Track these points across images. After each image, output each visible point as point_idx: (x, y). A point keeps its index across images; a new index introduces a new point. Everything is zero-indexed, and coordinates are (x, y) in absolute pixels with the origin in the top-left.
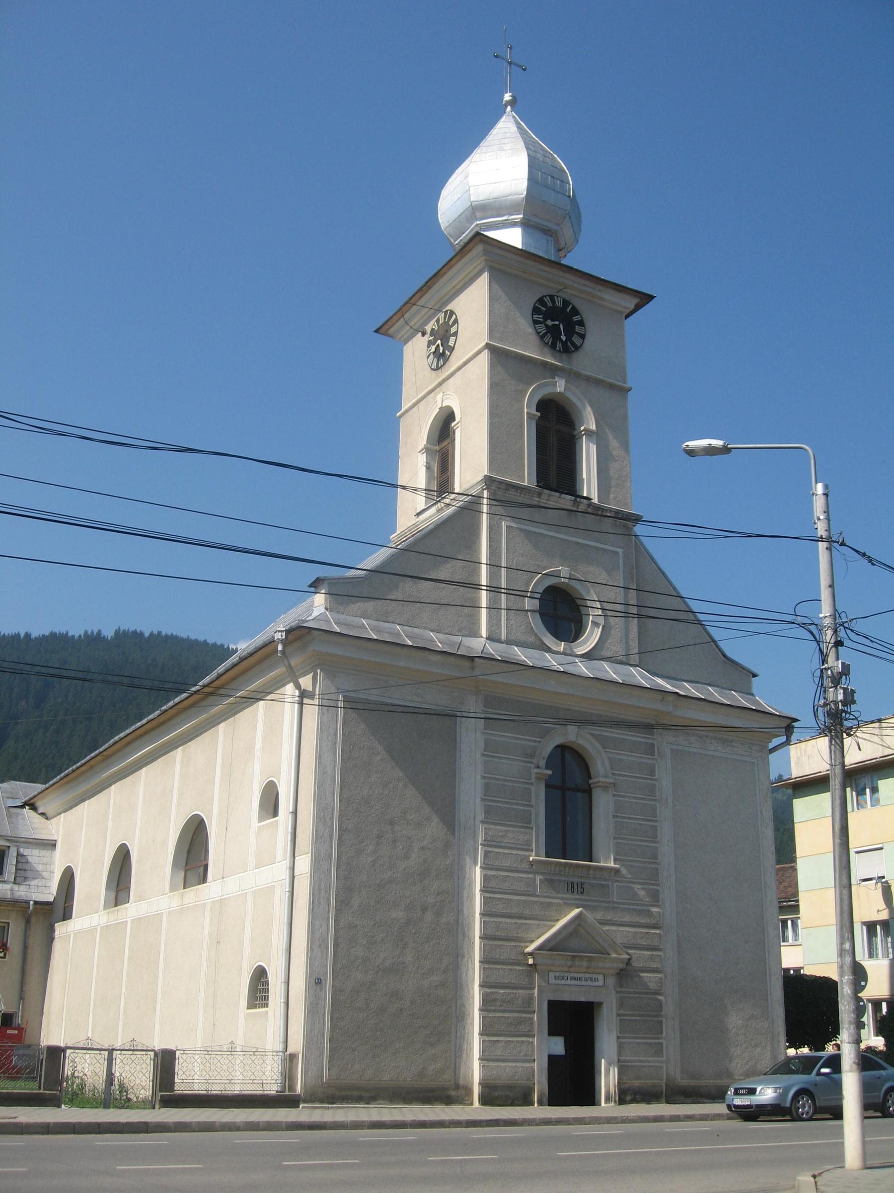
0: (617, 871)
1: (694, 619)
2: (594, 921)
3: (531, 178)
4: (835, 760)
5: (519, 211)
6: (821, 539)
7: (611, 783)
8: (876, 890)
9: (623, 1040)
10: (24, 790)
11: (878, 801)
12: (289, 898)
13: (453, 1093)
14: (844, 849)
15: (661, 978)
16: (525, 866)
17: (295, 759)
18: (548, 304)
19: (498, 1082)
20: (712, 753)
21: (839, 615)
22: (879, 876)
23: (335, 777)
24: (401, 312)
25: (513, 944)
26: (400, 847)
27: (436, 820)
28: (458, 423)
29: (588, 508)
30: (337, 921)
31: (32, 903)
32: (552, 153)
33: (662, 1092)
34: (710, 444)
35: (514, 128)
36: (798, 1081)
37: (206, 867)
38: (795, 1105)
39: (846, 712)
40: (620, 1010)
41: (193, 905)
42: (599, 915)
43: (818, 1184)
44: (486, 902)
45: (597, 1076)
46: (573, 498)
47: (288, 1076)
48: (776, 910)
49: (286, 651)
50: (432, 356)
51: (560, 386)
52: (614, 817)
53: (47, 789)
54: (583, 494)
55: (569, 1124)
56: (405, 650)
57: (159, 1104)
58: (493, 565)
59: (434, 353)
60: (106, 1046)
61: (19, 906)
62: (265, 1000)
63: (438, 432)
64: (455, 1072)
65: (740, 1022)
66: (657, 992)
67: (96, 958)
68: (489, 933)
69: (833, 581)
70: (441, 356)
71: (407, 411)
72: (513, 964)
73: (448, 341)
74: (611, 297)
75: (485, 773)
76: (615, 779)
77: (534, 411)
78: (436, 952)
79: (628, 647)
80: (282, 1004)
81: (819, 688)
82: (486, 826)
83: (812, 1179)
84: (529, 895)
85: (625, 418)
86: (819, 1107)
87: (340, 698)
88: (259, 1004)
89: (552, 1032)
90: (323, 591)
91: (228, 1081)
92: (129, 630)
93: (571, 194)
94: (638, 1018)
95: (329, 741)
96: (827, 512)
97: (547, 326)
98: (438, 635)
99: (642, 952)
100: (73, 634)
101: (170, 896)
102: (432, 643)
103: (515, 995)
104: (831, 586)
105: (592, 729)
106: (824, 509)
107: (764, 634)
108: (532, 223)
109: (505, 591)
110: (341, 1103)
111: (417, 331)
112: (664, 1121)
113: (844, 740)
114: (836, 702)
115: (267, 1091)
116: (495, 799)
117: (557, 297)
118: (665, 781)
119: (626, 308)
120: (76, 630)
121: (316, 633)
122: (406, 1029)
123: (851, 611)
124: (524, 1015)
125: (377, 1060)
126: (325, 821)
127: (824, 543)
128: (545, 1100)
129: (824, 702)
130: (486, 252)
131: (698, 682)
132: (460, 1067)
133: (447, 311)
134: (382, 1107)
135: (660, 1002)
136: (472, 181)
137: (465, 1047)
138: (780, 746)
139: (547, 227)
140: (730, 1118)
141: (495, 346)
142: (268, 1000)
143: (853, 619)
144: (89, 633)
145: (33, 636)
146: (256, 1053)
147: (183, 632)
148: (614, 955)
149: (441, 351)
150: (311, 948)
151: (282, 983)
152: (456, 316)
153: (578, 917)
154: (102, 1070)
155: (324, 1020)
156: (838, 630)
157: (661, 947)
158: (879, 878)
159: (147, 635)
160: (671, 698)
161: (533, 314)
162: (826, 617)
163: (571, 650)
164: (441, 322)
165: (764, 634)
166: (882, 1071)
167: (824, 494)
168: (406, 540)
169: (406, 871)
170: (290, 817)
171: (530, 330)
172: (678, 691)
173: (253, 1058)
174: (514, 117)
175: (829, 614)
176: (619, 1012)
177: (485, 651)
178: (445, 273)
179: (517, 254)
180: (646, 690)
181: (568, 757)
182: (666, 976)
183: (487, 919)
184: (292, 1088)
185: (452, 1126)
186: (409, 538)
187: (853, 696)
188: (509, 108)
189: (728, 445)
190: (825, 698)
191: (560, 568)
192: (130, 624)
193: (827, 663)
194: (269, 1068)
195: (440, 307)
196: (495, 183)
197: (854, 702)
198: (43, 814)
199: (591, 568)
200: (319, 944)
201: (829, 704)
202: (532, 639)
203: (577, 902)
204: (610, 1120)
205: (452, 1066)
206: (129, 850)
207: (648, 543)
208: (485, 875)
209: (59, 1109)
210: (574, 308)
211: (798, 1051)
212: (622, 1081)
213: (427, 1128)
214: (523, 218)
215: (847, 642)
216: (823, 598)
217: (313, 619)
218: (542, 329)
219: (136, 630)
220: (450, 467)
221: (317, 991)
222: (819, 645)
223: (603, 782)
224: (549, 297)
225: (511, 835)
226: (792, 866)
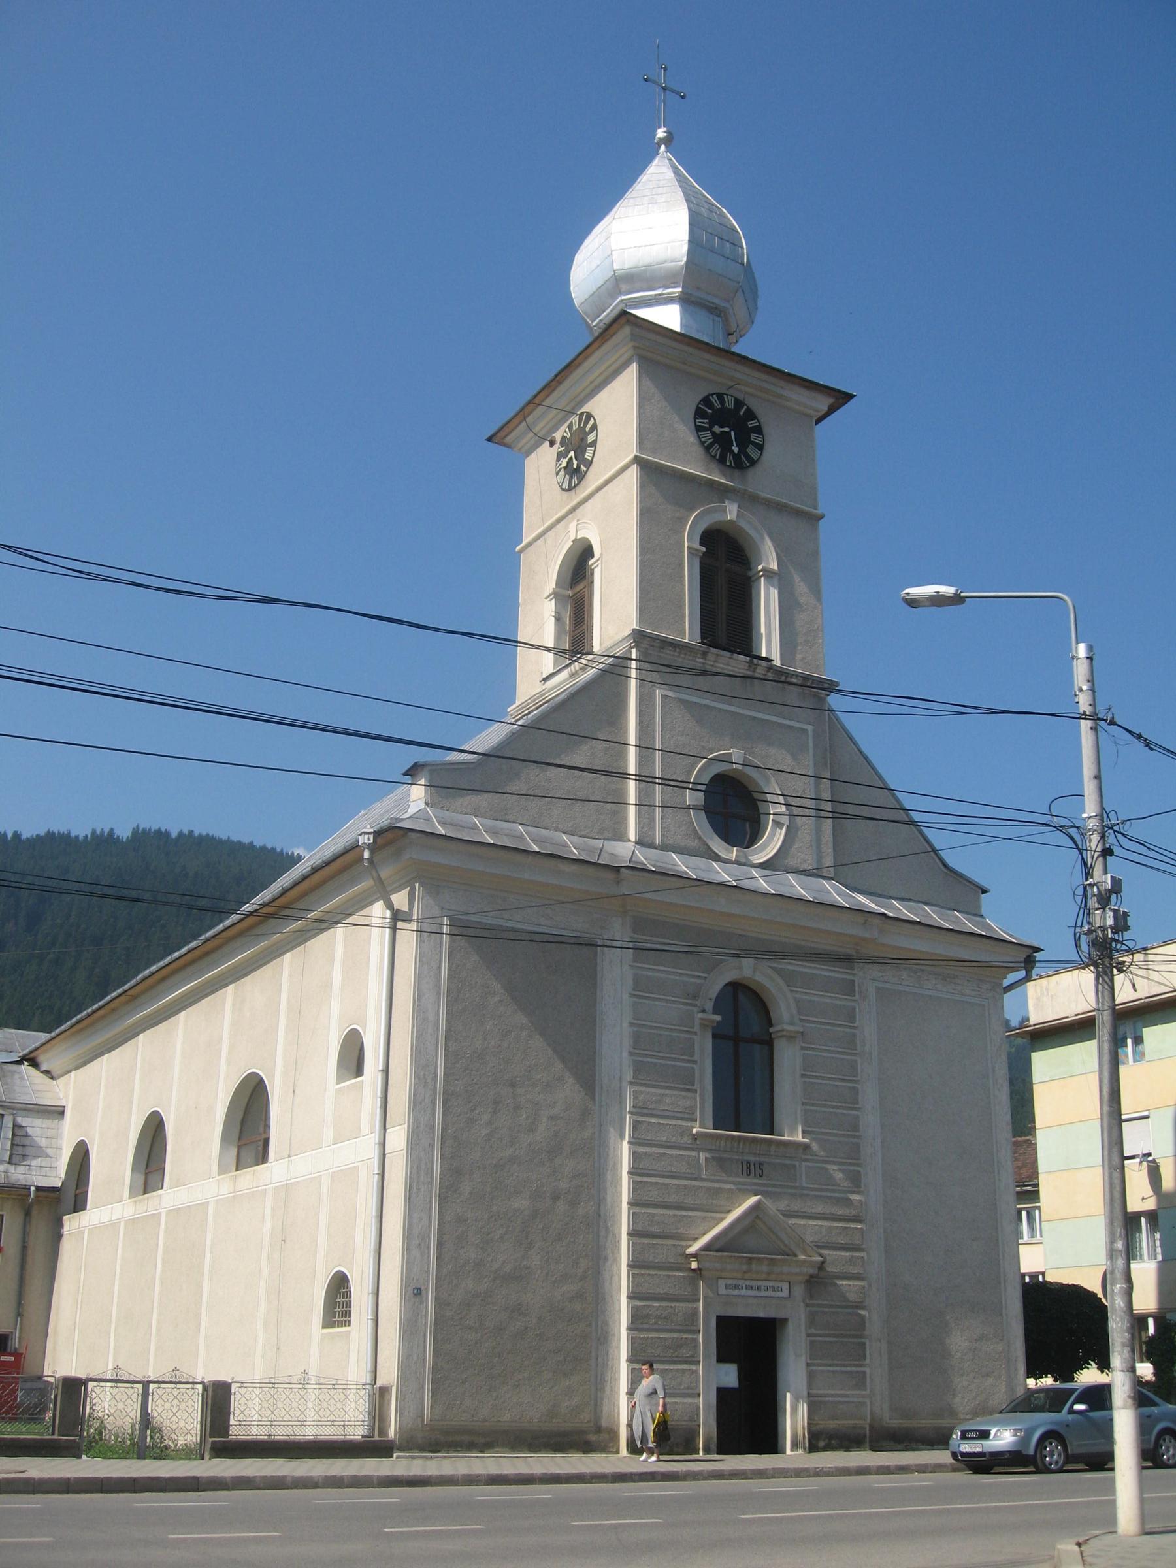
0: (806, 1147)
1: (907, 819)
2: (777, 1212)
3: (693, 241)
4: (1103, 1004)
5: (677, 283)
6: (1084, 716)
7: (798, 1032)
8: (1140, 1171)
10: (21, 1041)
11: (1143, 1054)
12: (378, 1182)
13: (593, 1438)
14: (1115, 1119)
15: (864, 1287)
16: (686, 1140)
17: (386, 1000)
18: (716, 404)
20: (930, 993)
21: (1108, 814)
22: (1144, 1152)
24: (523, 413)
26: (524, 1116)
27: (570, 1080)
28: (598, 560)
29: (768, 671)
31: (33, 1189)
33: (865, 1436)
34: (938, 592)
35: (670, 175)
36: (1044, 1420)
37: (266, 1142)
38: (1041, 1453)
39: (1117, 941)
40: (810, 1328)
41: (250, 1192)
42: (783, 1205)
43: (1084, 1555)
44: (636, 1187)
45: (780, 1414)
46: (748, 658)
47: (378, 1416)
48: (1012, 1198)
49: (375, 860)
50: (562, 472)
51: (731, 512)
52: (803, 1076)
54: (761, 653)
55: (746, 1478)
56: (530, 858)
57: (210, 1454)
58: (645, 748)
59: (565, 468)
60: (140, 1378)
61: (15, 1193)
62: (346, 1317)
63: (571, 572)
64: (595, 1410)
65: (967, 1343)
66: (860, 1305)
67: (119, 1261)
68: (640, 1229)
69: (1099, 770)
70: (575, 473)
71: (530, 544)
72: (671, 1268)
73: (584, 452)
76: (803, 1026)
77: (697, 545)
79: (820, 856)
81: (1082, 910)
82: (637, 1088)
83: (1076, 1548)
84: (691, 1179)
85: (816, 554)
86: (1072, 1454)
87: (446, 921)
88: (338, 1322)
89: (721, 1359)
90: (422, 782)
92: (150, 829)
93: (745, 261)
94: (835, 1339)
96: (1091, 680)
97: (713, 433)
98: (572, 837)
99: (839, 1253)
100: (77, 834)
101: (218, 1180)
102: (568, 848)
103: (675, 1310)
104: (1097, 777)
106: (1088, 677)
107: (1010, 839)
108: (693, 299)
109: (660, 781)
110: (448, 1452)
111: (543, 439)
112: (870, 1474)
113: (1115, 977)
114: (1103, 928)
115: (350, 1435)
116: (646, 1052)
117: (727, 395)
118: (868, 1029)
120: (80, 829)
123: (1122, 810)
124: (685, 1336)
125: (495, 1394)
126: (425, 1082)
127: (1088, 721)
128: (714, 1446)
129: (1089, 928)
130: (634, 337)
131: (910, 900)
133: (583, 413)
134: (501, 1457)
135: (862, 1318)
136: (615, 243)
137: (608, 1378)
138: (1019, 983)
139: (713, 303)
140: (955, 1470)
142: (350, 1316)
143: (1126, 821)
144: (98, 832)
145: (24, 837)
146: (336, 1386)
147: (221, 831)
148: (802, 1257)
149: (575, 466)
150: (407, 1249)
151: (369, 1294)
153: (756, 1207)
154: (133, 1413)
155: (425, 1342)
156: (1107, 834)
157: (864, 1246)
158: (1145, 1155)
159: (174, 835)
160: (877, 921)
161: (695, 419)
162: (1091, 817)
163: (746, 857)
164: (574, 429)
165: (1010, 839)
166: (1153, 1408)
167: (1088, 658)
168: (529, 713)
170: (380, 1077)
171: (692, 439)
172: (886, 912)
173: (332, 1392)
174: (669, 159)
175: (1094, 814)
177: (634, 859)
178: (580, 364)
179: (676, 340)
180: (845, 910)
181: (742, 997)
182: (870, 1285)
183: (637, 1210)
184: (383, 1431)
185: (594, 1481)
186: (533, 711)
187: (1126, 921)
188: (663, 148)
189: (961, 592)
190: (1089, 923)
191: (731, 751)
192: (152, 821)
193: (1092, 878)
194: (310, 1405)
195: (573, 409)
196: (646, 246)
197: (1127, 928)
198: (47, 1072)
199: (772, 751)
200: (418, 1242)
201: (1095, 931)
202: (694, 843)
203: (754, 1187)
204: (799, 1473)
206: (162, 1119)
207: (850, 722)
208: (634, 1153)
209: (79, 1460)
210: (749, 411)
211: (1038, 1381)
213: (561, 1484)
215: (1117, 850)
216: (1086, 793)
217: (410, 817)
218: (707, 437)
219: (160, 829)
220: (586, 617)
221: (416, 1305)
222: (1081, 854)
223: (787, 1031)
224: (717, 396)
225: (668, 1100)
226: (1028, 1140)
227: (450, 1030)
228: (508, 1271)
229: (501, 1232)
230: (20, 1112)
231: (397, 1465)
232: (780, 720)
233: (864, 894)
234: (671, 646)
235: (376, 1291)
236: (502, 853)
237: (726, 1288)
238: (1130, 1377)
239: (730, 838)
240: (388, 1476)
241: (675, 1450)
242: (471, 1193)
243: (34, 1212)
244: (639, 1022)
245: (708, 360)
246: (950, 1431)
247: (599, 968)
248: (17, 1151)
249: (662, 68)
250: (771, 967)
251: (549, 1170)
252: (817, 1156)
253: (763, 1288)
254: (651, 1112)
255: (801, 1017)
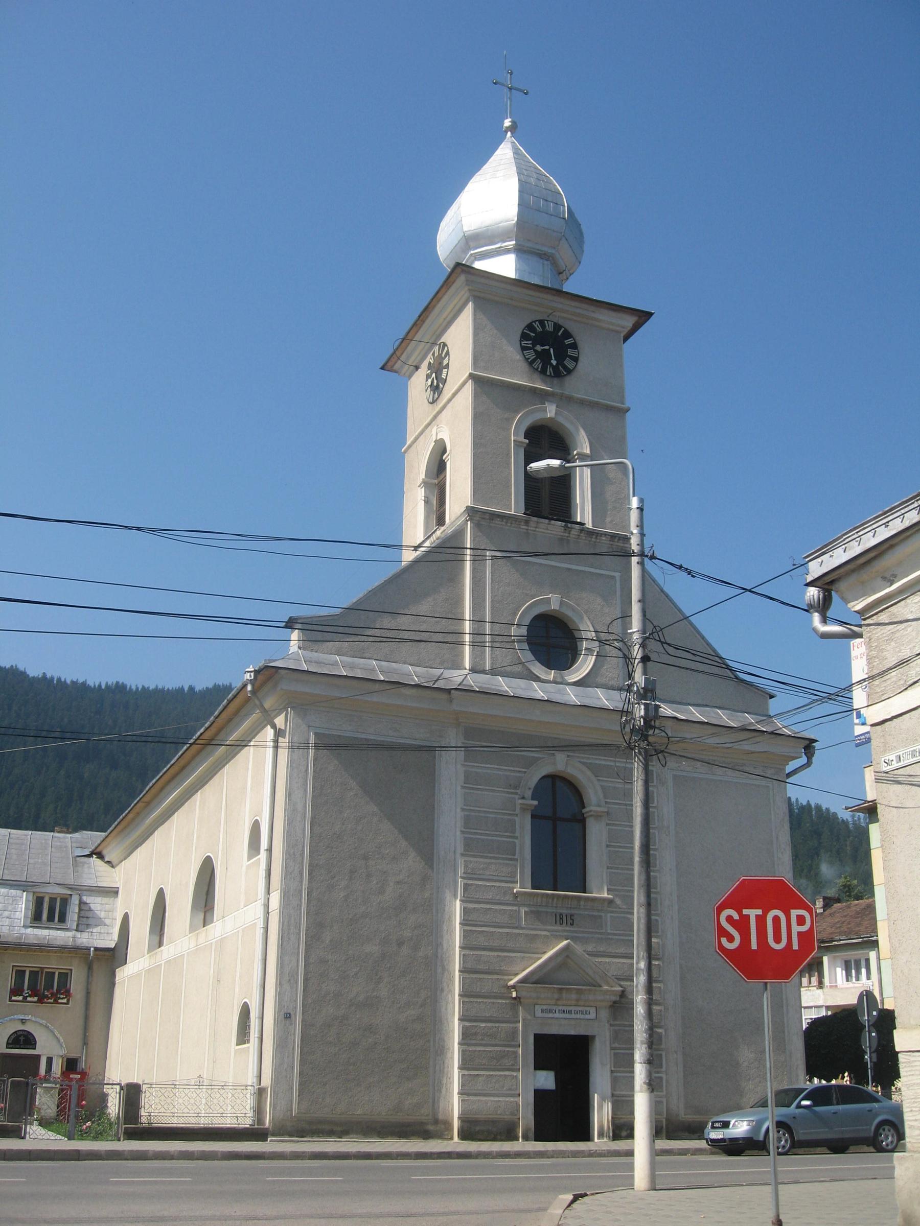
0: (610, 902)
2: (583, 952)
3: (522, 204)
9: (619, 1074)
13: (431, 1128)
15: (661, 1011)
16: (509, 898)
18: (537, 328)
19: (479, 1116)
23: (305, 814)
25: (495, 977)
27: (412, 854)
28: (448, 455)
30: (307, 958)
31: (92, 949)
32: (548, 175)
40: (614, 1043)
44: (466, 935)
45: (591, 1111)
47: (259, 1110)
51: (551, 411)
52: (607, 846)
53: (106, 837)
64: (433, 1106)
65: (752, 1055)
70: (436, 389)
71: (410, 446)
72: (495, 997)
74: (606, 317)
75: (464, 805)
77: (521, 438)
78: (413, 986)
80: (256, 1039)
84: (513, 928)
86: (798, 1141)
89: (538, 1066)
91: (219, 1115)
95: (299, 778)
97: (536, 351)
105: (583, 758)
108: (525, 249)
110: (312, 1137)
117: (548, 321)
119: (623, 327)
121: (283, 672)
122: (381, 1063)
124: (507, 1049)
125: (350, 1094)
130: (468, 282)
131: (707, 706)
132: (438, 1101)
137: (444, 1082)
139: (542, 251)
140: (712, 1153)
141: (479, 375)
145: (197, 689)
146: (225, 1087)
150: (280, 984)
152: (448, 348)
153: (566, 948)
155: (293, 1054)
157: (660, 979)
161: (521, 341)
163: (562, 677)
169: (381, 905)
171: (518, 357)
176: (614, 1046)
178: (435, 306)
183: (467, 952)
185: (399, 1158)
188: (509, 134)
194: (204, 1101)
195: (435, 341)
198: (109, 862)
200: (288, 978)
203: (566, 934)
205: (431, 1101)
208: (465, 908)
212: (616, 1116)
214: (516, 244)
218: (531, 355)
223: (594, 811)
227: (315, 818)
228: (361, 1000)
229: (355, 970)
230: (85, 893)
231: (269, 1146)
232: (592, 570)
233: (665, 702)
234: (498, 518)
235: (261, 1016)
236: (354, 682)
237: (542, 1012)
238: (646, 1068)
239: (549, 664)
240: (230, 1152)
241: (499, 1137)
242: (331, 941)
243: (95, 966)
244: (468, 808)
245: (530, 295)
246: (707, 1123)
247: (437, 767)
248: (83, 921)
249: (508, 73)
250: (580, 762)
251: (395, 922)
252: (620, 908)
253: (573, 1012)
254: (479, 877)
255: (606, 800)
